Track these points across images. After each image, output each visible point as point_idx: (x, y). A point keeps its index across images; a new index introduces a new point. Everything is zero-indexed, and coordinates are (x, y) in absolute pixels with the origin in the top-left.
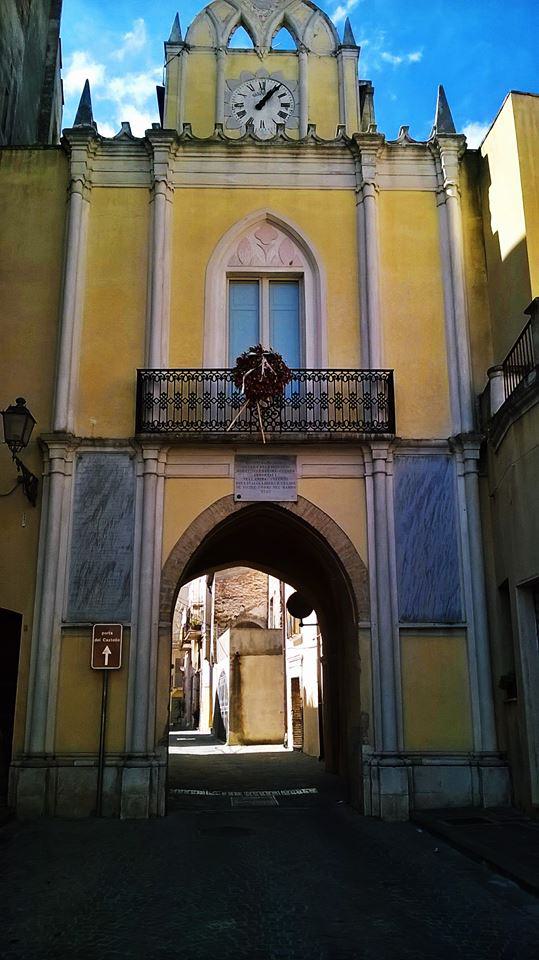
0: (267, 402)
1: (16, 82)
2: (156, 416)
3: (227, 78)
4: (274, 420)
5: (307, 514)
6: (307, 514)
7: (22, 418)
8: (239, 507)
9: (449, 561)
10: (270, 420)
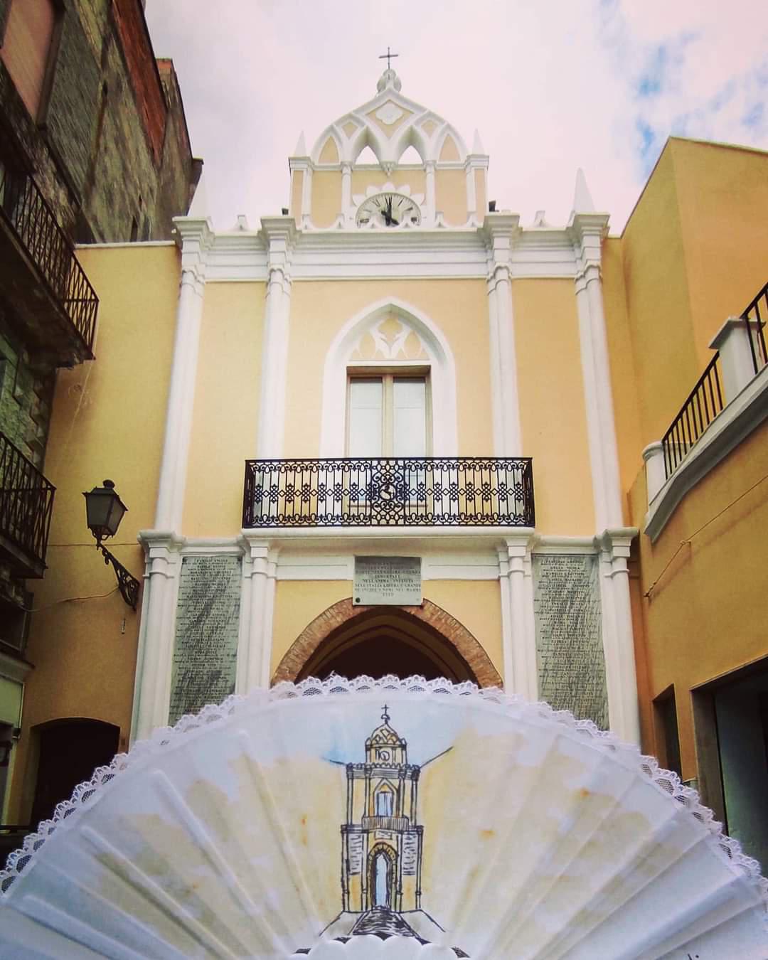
0: (390, 494)
1: (147, 220)
2: (266, 507)
3: (354, 222)
4: (397, 513)
5: (434, 618)
6: (434, 618)
7: (107, 501)
8: (358, 611)
9: (216, 932)
10: (383, 471)
